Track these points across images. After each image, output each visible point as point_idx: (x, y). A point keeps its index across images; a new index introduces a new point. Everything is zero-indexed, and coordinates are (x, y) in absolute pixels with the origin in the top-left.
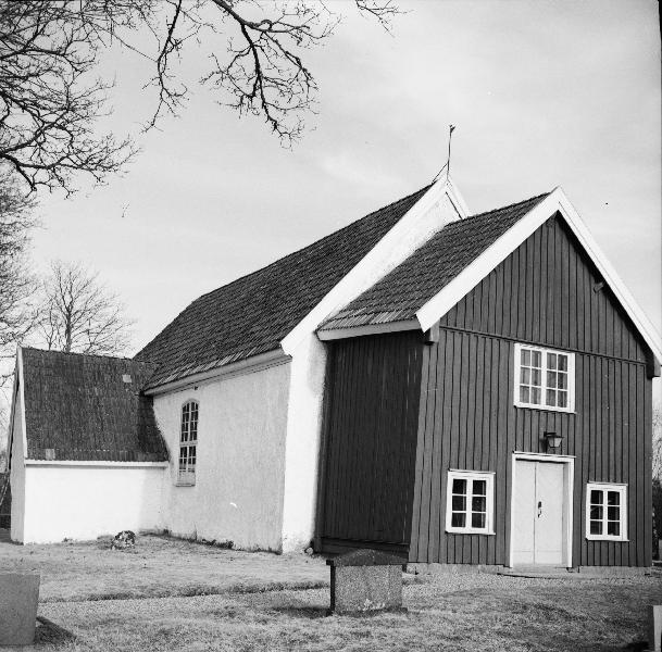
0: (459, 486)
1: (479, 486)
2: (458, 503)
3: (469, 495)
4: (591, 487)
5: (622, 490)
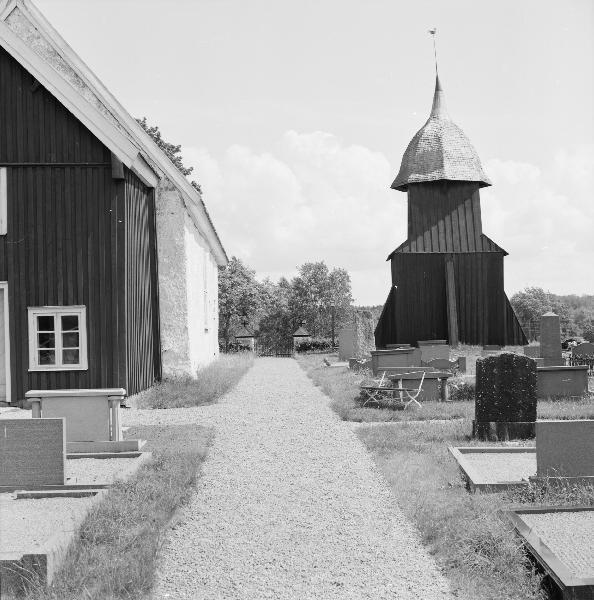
0: (46, 323)
1: (70, 323)
2: (46, 341)
3: (58, 331)
4: (33, 315)
5: (80, 312)
